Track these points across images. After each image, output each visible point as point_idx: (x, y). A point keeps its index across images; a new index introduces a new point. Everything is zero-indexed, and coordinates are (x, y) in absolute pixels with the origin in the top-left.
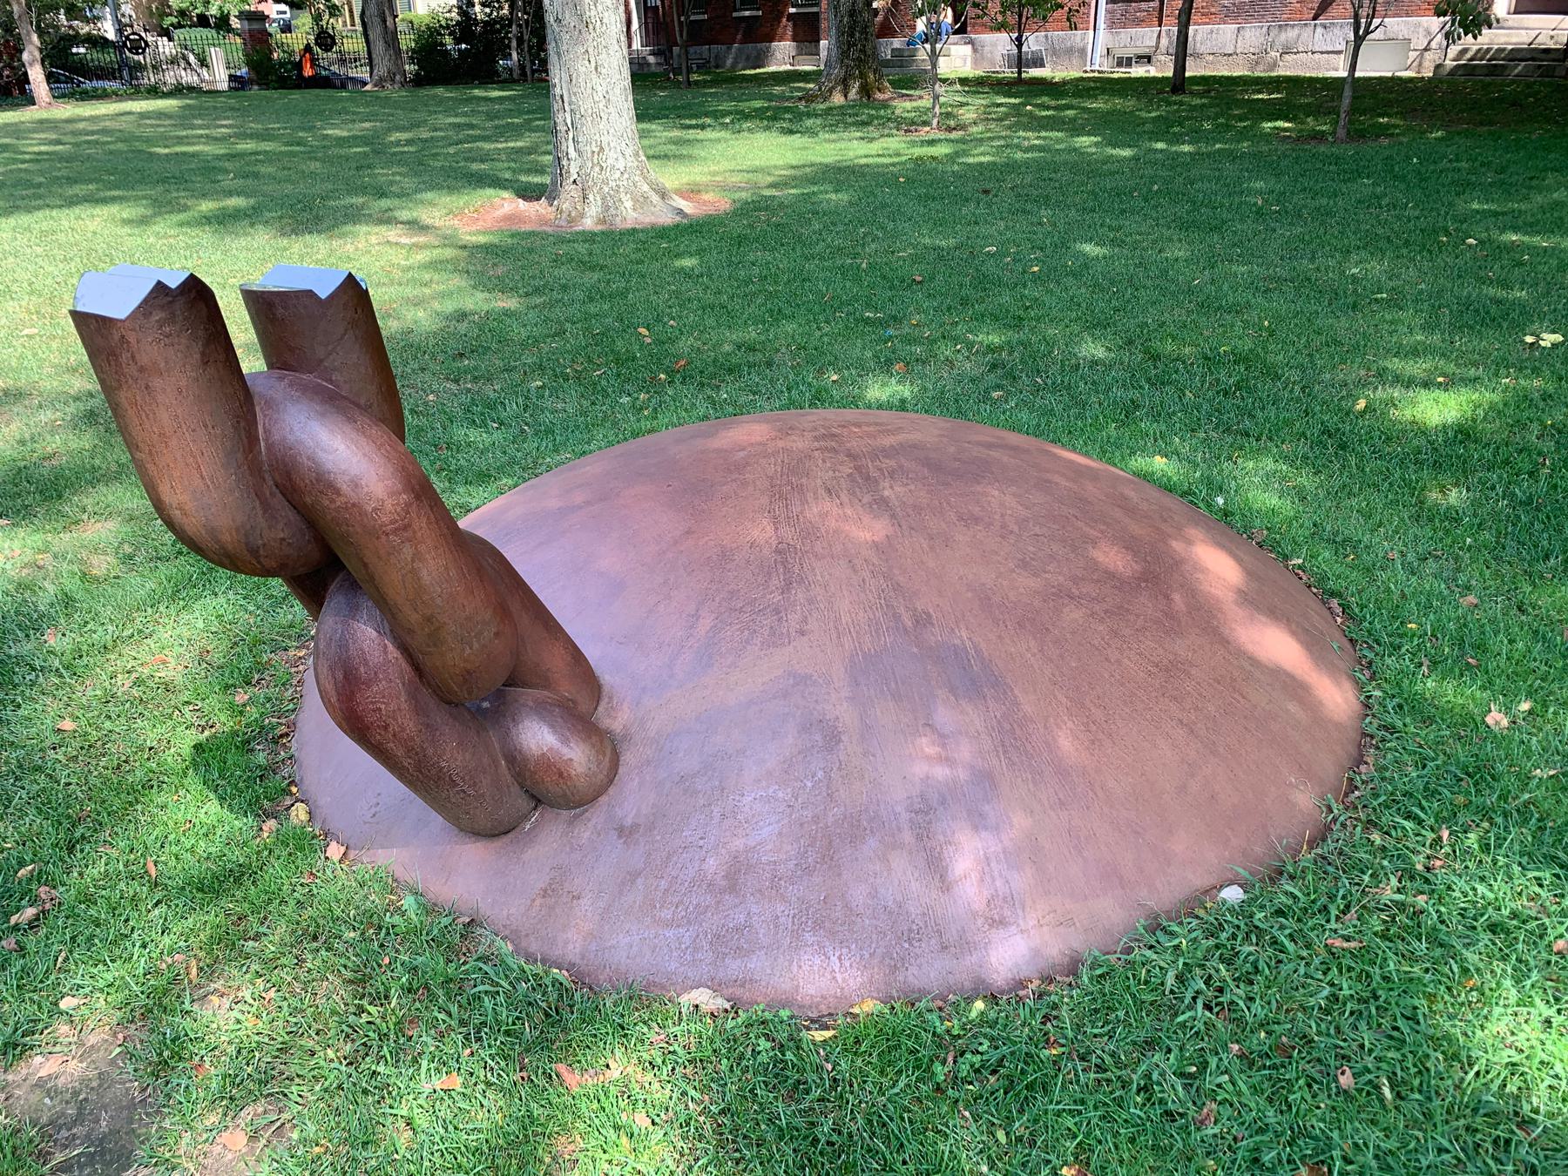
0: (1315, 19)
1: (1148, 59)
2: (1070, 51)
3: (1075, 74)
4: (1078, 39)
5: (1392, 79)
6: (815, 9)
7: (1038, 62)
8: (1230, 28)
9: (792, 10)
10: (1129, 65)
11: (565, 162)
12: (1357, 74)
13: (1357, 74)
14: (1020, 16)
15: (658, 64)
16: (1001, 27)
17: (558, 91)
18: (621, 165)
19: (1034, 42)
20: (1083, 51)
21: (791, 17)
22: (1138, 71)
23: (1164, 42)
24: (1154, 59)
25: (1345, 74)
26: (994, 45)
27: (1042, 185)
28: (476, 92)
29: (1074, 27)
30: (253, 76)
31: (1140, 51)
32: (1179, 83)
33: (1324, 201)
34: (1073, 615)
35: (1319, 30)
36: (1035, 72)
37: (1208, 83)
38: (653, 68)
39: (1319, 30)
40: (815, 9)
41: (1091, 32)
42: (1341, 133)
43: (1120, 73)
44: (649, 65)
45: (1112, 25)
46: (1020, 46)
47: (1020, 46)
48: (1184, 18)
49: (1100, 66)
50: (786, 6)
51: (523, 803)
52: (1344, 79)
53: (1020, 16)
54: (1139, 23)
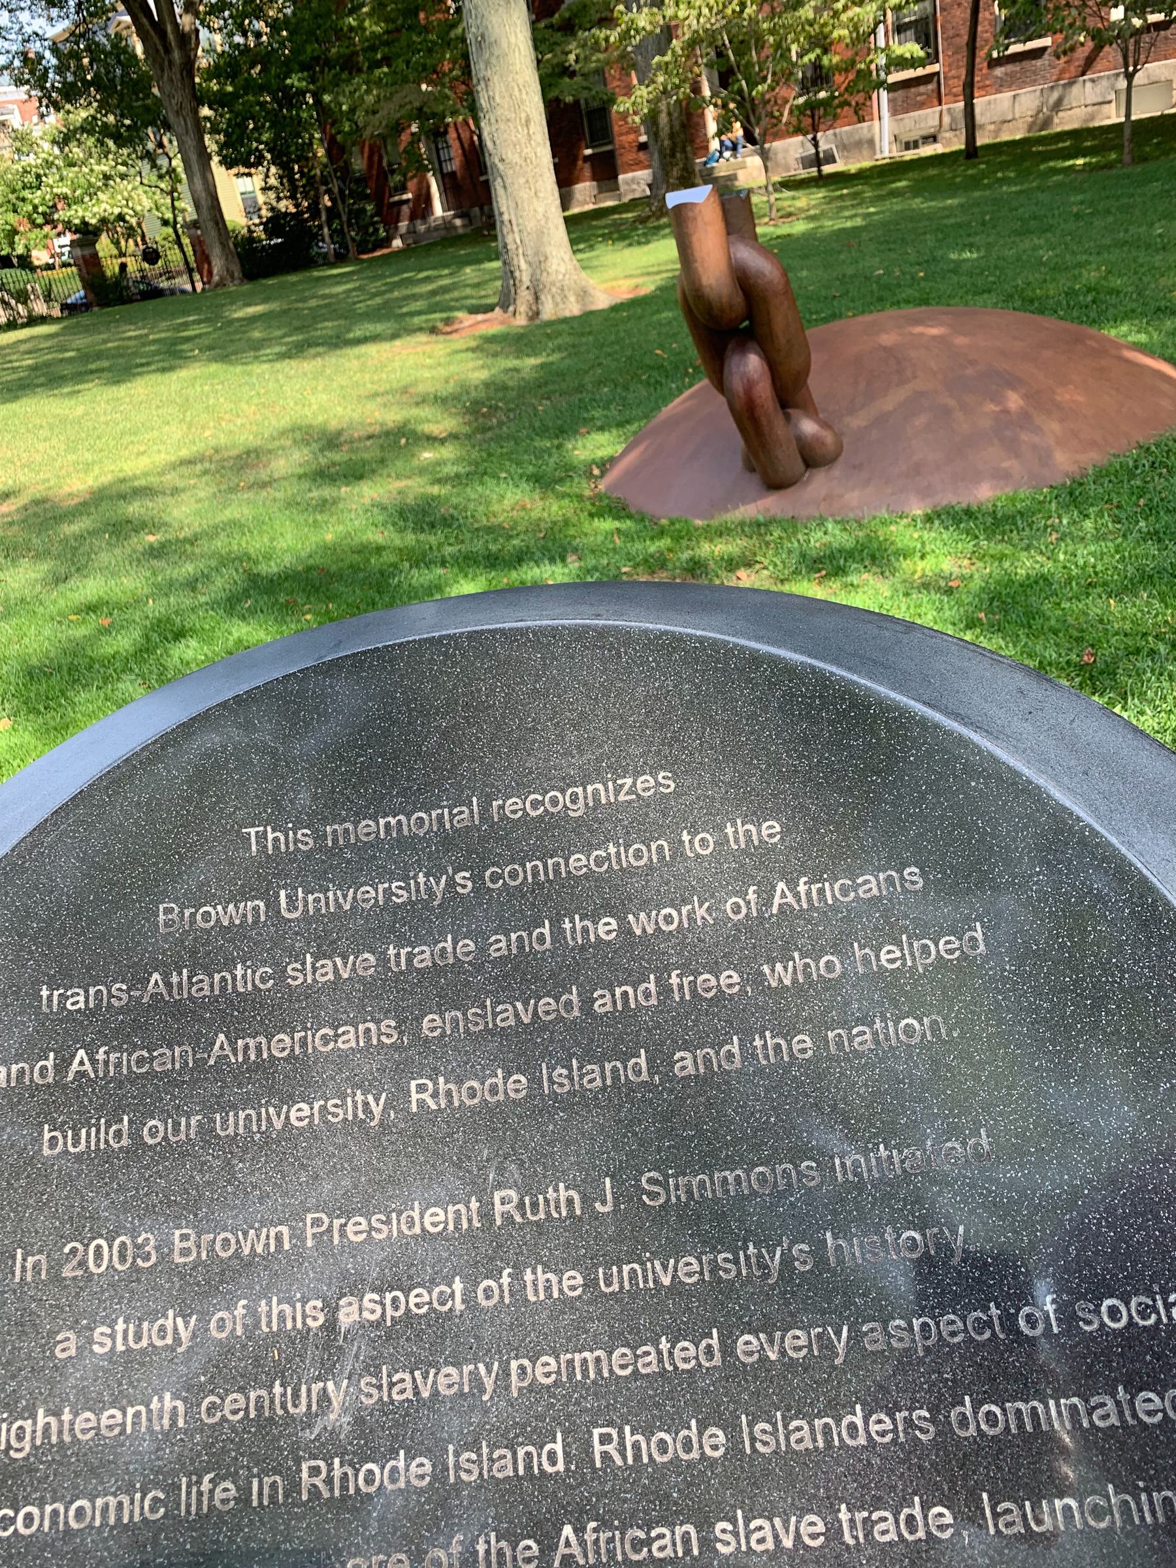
0: (1083, 74)
1: (933, 138)
2: (859, 144)
3: (867, 164)
4: (865, 131)
5: (1162, 116)
6: (609, 148)
7: (831, 159)
8: (1007, 95)
9: (588, 152)
10: (916, 145)
11: (517, 274)
12: (1133, 118)
13: (1133, 118)
14: (813, 117)
15: (464, 226)
16: (798, 131)
17: (506, 217)
18: (562, 269)
19: (826, 141)
20: (871, 142)
21: (587, 159)
22: (927, 151)
23: (946, 120)
24: (939, 137)
25: (1123, 119)
26: (786, 151)
27: (889, 235)
28: (316, 274)
29: (861, 120)
30: (91, 296)
31: (925, 133)
32: (971, 151)
33: (1126, 200)
34: (1047, 353)
35: (1089, 85)
36: (827, 169)
37: (996, 148)
38: (461, 231)
39: (1089, 85)
40: (609, 148)
41: (876, 122)
42: (1127, 158)
43: (909, 155)
44: (455, 228)
45: (894, 112)
46: (816, 145)
47: (816, 145)
48: (968, 91)
49: (887, 151)
50: (579, 149)
51: (802, 466)
52: (1121, 124)
53: (813, 117)
54: (921, 106)
